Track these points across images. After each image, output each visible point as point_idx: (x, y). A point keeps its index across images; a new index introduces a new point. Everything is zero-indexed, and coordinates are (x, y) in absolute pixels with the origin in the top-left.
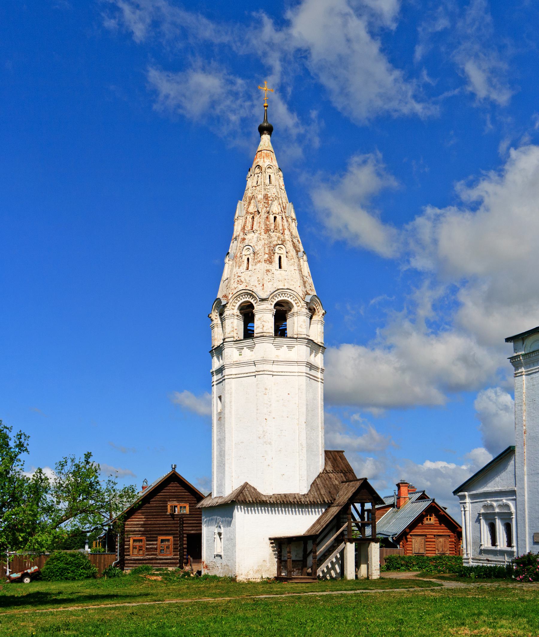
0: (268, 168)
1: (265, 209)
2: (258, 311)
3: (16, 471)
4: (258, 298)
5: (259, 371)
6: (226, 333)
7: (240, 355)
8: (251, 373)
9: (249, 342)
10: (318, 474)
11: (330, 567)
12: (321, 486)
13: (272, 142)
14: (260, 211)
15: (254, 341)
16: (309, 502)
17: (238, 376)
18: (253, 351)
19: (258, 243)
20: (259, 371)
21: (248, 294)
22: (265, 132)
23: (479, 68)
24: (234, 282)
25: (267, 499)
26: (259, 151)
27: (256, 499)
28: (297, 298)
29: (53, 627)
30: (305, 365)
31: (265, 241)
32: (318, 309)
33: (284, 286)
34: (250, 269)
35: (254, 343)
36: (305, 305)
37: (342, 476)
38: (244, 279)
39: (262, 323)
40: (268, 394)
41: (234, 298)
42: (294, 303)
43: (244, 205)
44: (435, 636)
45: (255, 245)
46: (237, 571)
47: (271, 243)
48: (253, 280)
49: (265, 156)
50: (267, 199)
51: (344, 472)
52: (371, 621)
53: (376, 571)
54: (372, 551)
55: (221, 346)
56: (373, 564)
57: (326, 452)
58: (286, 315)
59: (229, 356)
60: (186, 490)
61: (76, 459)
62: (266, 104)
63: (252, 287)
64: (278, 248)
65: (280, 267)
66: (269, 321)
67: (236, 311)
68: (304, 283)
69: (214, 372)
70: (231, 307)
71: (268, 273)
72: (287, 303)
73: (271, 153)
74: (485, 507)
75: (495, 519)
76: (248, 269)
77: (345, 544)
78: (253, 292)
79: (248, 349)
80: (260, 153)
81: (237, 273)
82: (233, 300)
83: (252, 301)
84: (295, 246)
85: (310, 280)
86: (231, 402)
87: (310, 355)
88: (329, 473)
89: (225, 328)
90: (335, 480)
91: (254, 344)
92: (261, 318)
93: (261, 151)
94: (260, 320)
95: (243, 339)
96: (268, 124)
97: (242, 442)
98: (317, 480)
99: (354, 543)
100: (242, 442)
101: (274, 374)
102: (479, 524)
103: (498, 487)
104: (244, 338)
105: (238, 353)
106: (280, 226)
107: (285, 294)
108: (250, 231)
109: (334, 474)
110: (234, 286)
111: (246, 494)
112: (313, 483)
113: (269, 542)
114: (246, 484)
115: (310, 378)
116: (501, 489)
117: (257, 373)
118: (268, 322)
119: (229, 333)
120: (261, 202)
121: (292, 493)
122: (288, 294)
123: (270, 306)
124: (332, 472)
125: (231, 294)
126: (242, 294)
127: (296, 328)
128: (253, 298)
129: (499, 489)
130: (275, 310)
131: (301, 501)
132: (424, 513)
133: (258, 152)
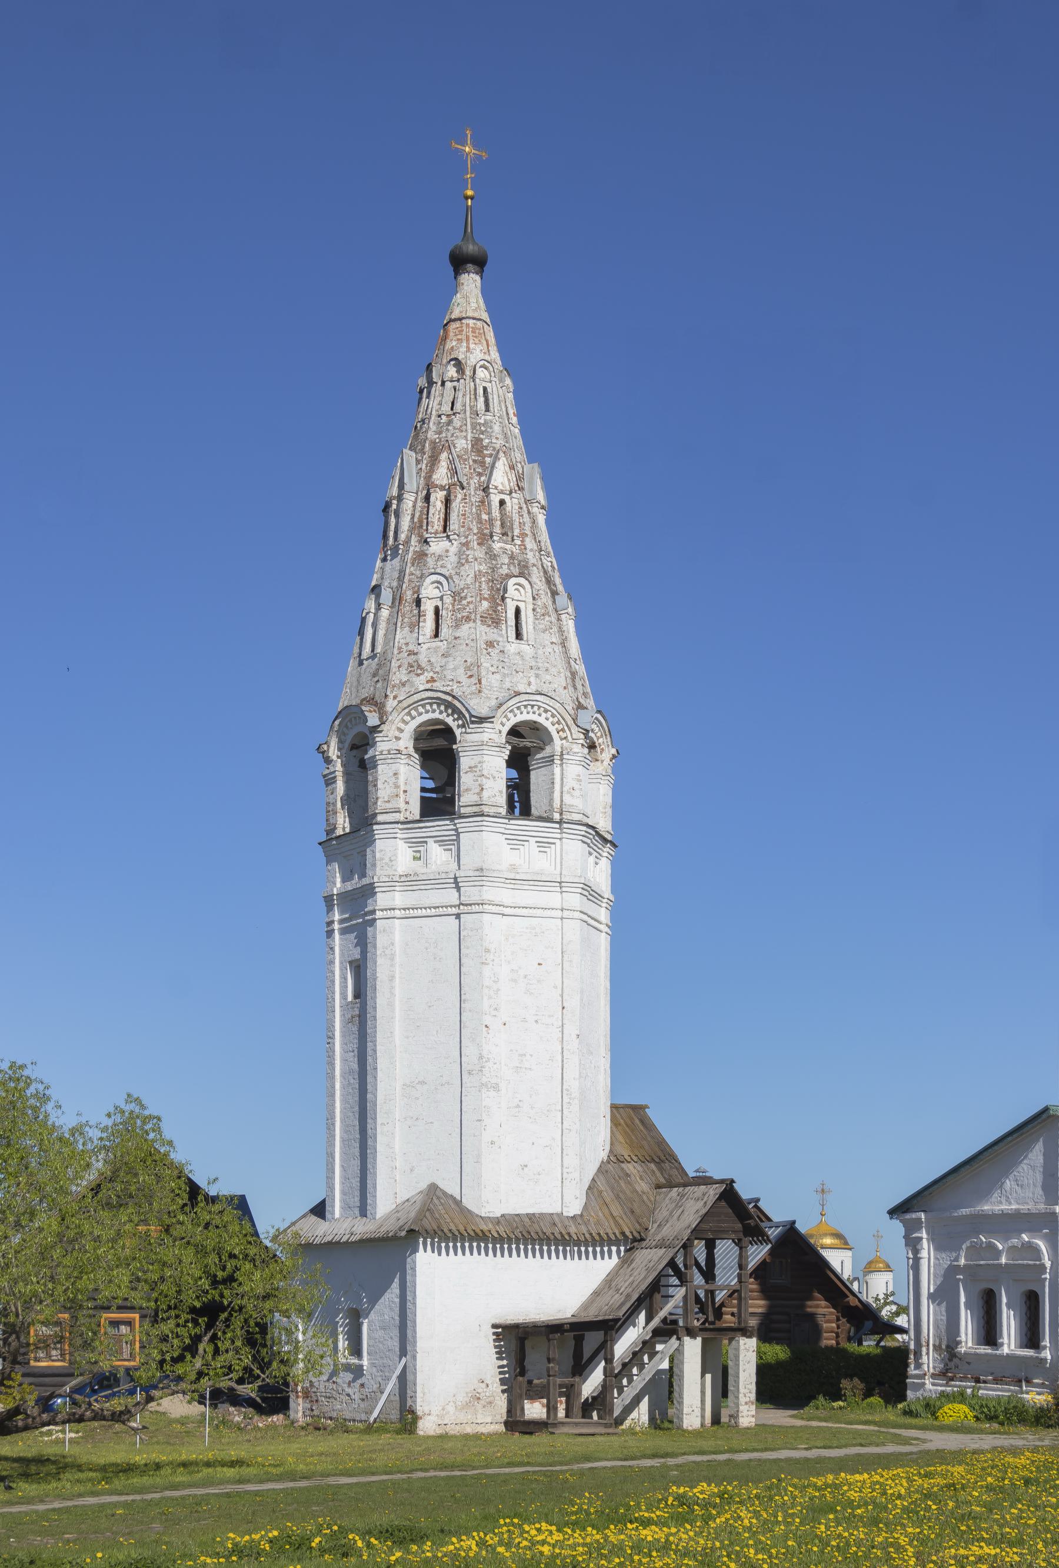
0: (481, 367)
1: (476, 479)
2: (467, 749)
3: (876, 1234)
5: (470, 905)
6: (377, 799)
8: (446, 907)
9: (441, 826)
10: (597, 1165)
11: (636, 1368)
12: (608, 1196)
13: (485, 292)
14: (465, 484)
15: (455, 825)
16: (587, 1236)
17: (410, 913)
19: (462, 568)
20: (470, 905)
21: (448, 705)
22: (470, 267)
24: (399, 667)
25: (491, 1226)
26: (455, 320)
27: (465, 1227)
28: (561, 719)
30: (580, 890)
31: (480, 564)
32: (600, 746)
33: (529, 684)
36: (582, 736)
37: (653, 1172)
38: (426, 660)
39: (477, 780)
40: (491, 963)
42: (552, 730)
43: (418, 462)
45: (453, 572)
46: (418, 1404)
47: (494, 571)
48: (451, 666)
49: (471, 334)
51: (657, 1160)
52: (311, 1552)
53: (747, 1407)
54: (741, 1358)
55: (610, 1323)
56: (742, 1390)
58: (529, 758)
59: (387, 860)
60: (935, 1291)
61: (550, 1437)
62: (470, 193)
63: (451, 683)
64: (433, 583)
65: (519, 636)
66: (496, 774)
67: (407, 743)
68: (574, 674)
69: (335, 897)
71: (490, 650)
72: (535, 728)
73: (486, 326)
78: (454, 697)
80: (457, 324)
81: (407, 644)
83: (449, 720)
84: (549, 581)
85: (581, 669)
86: (392, 978)
88: (623, 1162)
89: (375, 786)
90: (640, 1182)
92: (476, 767)
93: (460, 319)
95: (418, 817)
96: (476, 248)
97: (423, 1083)
98: (596, 1179)
99: (699, 1340)
100: (423, 1083)
103: (1010, 1203)
105: (410, 853)
106: (514, 527)
107: (533, 706)
108: (438, 536)
109: (635, 1164)
111: (440, 1214)
112: (590, 1188)
114: (433, 1188)
115: (588, 925)
116: (1019, 1210)
118: (494, 778)
120: (465, 460)
121: (544, 1211)
123: (496, 734)
124: (629, 1159)
126: (423, 700)
127: (559, 794)
128: (457, 719)
129: (1013, 1207)
130: (510, 748)
131: (569, 1234)
132: (567, 1327)
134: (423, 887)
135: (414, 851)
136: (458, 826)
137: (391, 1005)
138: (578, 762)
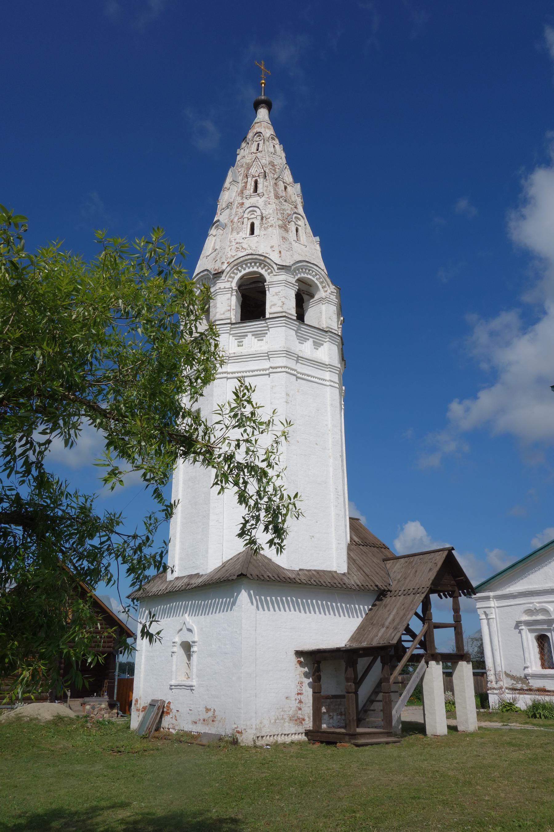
4: (274, 266)
6: (217, 313)
7: (238, 346)
15: (267, 323)
18: (262, 340)
23: (346, 742)
29: (418, 820)
34: (260, 190)
35: (267, 326)
41: (234, 266)
42: (320, 287)
44: (1, 248)
50: (273, 166)
57: (350, 518)
70: (227, 278)
74: (529, 612)
75: (346, 730)
76: (256, 192)
77: (427, 663)
79: (253, 337)
82: (231, 269)
87: (161, 631)
91: (267, 328)
92: (279, 292)
94: (277, 295)
95: (240, 321)
101: (229, 376)
102: (520, 634)
104: (241, 320)
110: (231, 254)
113: (293, 659)
117: (271, 370)
119: (222, 313)
122: (313, 271)
125: (226, 262)
126: (246, 260)
133: (256, 123)
134: (245, 360)
135: (238, 342)
136: (268, 323)
137: (177, 491)
138: (334, 304)
